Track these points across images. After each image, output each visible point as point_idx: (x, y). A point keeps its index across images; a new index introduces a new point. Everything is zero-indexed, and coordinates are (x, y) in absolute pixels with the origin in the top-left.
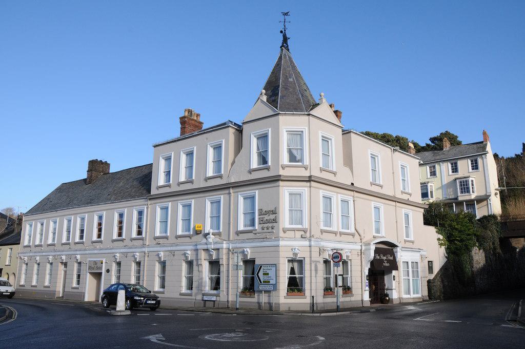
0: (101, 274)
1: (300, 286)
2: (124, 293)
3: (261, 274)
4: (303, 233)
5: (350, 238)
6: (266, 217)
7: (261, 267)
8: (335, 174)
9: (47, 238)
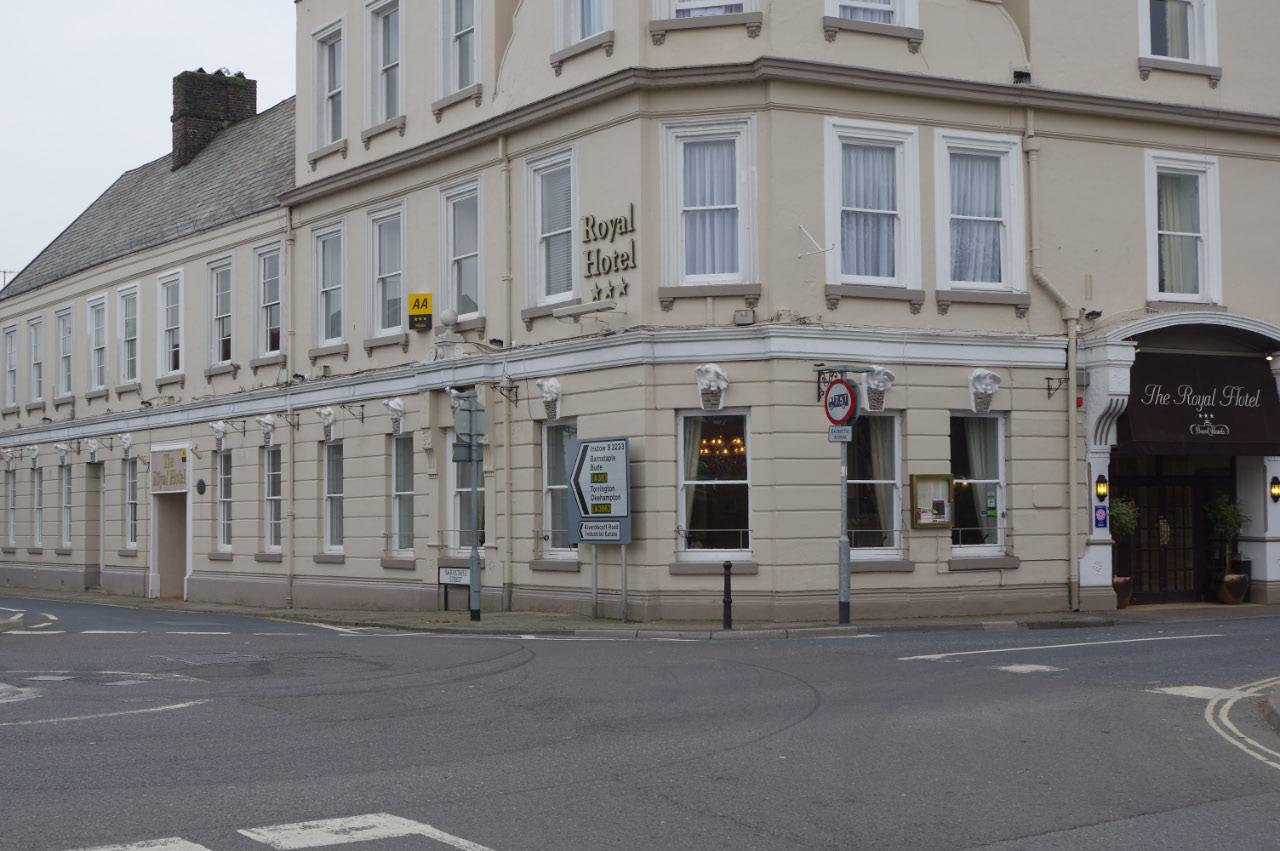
0: (183, 496)
1: (883, 526)
2: (732, 585)
3: (585, 479)
4: (741, 305)
5: (1004, 322)
6: (607, 249)
7: (586, 448)
8: (1212, 78)
9: (48, 380)
